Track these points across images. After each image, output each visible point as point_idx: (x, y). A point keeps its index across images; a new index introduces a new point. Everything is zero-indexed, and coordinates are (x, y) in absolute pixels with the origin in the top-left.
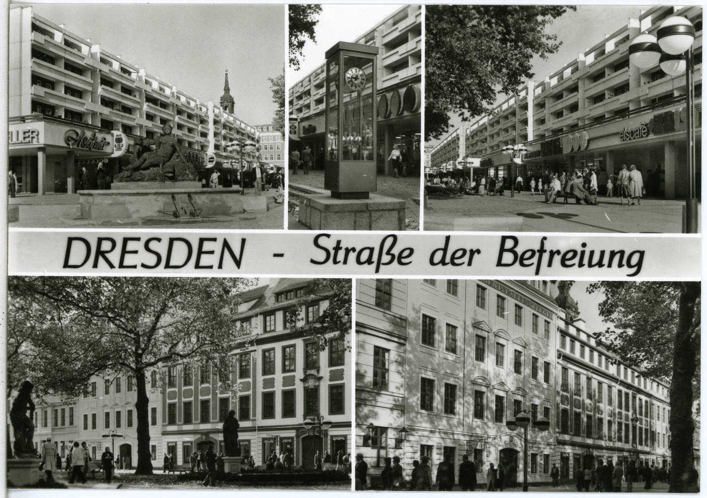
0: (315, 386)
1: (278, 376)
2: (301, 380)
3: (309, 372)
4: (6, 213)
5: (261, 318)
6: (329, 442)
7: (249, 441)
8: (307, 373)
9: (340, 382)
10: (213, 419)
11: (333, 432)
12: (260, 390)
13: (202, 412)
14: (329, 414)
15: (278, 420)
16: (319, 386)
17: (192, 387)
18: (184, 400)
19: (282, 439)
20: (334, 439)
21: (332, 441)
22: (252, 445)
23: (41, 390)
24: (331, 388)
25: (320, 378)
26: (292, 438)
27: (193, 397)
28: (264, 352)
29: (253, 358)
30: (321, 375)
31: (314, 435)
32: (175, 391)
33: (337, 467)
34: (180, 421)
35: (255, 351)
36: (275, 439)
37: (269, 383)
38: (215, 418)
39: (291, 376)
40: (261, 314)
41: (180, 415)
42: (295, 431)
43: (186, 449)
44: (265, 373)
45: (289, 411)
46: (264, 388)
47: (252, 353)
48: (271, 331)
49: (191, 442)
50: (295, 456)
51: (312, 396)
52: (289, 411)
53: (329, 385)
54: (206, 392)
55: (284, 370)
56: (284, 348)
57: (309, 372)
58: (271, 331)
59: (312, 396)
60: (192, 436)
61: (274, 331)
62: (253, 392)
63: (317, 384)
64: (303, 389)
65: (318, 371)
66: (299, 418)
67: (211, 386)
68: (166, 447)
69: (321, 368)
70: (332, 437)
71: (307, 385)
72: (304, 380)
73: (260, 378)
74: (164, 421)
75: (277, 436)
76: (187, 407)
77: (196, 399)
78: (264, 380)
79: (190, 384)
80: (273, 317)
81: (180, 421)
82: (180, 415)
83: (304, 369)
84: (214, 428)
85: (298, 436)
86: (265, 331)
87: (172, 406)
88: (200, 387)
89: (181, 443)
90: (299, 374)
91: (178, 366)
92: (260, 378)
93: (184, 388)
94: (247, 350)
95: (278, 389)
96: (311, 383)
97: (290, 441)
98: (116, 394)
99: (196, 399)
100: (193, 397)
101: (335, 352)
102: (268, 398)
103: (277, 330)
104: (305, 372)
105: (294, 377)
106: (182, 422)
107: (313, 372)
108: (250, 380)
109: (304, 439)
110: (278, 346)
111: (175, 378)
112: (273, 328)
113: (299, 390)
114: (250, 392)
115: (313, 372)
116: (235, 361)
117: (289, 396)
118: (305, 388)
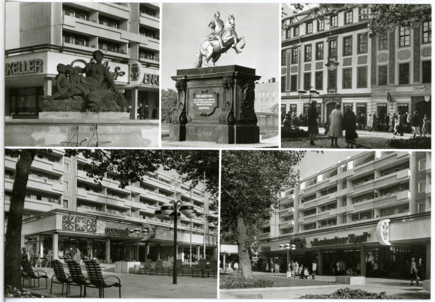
0: (334, 69)
1: (314, 62)
2: (326, 65)
3: (331, 60)
4: (4, 131)
5: (304, 24)
7: (296, 105)
8: (330, 60)
10: (287, 89)
12: (303, 71)
15: (354, 90)
16: (336, 69)
18: (291, 74)
21: (344, 107)
22: (298, 108)
24: (344, 70)
25: (337, 64)
27: (286, 73)
28: (306, 46)
29: (299, 51)
30: (338, 62)
31: (333, 102)
32: (285, 68)
33: (390, 130)
34: (288, 89)
35: (300, 46)
39: (364, 56)
40: (304, 22)
41: (288, 85)
42: (322, 99)
44: (344, 54)
45: (319, 86)
46: (305, 70)
47: (299, 48)
48: (310, 33)
53: (357, 67)
54: (294, 69)
55: (359, 52)
57: (331, 60)
58: (297, 35)
61: (312, 33)
63: (335, 68)
64: (327, 71)
65: (336, 59)
66: (324, 92)
70: (344, 104)
71: (330, 68)
72: (328, 65)
73: (303, 64)
76: (346, 73)
77: (288, 75)
78: (305, 65)
79: (296, 63)
81: (288, 89)
82: (288, 85)
83: (328, 58)
85: (324, 103)
86: (307, 33)
90: (325, 61)
91: (287, 50)
92: (303, 64)
93: (291, 66)
94: (296, 46)
95: (313, 71)
96: (332, 67)
99: (288, 75)
100: (286, 73)
101: (347, 46)
103: (325, 30)
104: (329, 60)
105: (322, 63)
106: (290, 90)
107: (333, 60)
108: (297, 65)
109: (328, 105)
110: (313, 42)
111: (285, 59)
112: (311, 32)
113: (325, 70)
114: (297, 73)
115: (333, 60)
116: (302, 49)
117: (319, 75)
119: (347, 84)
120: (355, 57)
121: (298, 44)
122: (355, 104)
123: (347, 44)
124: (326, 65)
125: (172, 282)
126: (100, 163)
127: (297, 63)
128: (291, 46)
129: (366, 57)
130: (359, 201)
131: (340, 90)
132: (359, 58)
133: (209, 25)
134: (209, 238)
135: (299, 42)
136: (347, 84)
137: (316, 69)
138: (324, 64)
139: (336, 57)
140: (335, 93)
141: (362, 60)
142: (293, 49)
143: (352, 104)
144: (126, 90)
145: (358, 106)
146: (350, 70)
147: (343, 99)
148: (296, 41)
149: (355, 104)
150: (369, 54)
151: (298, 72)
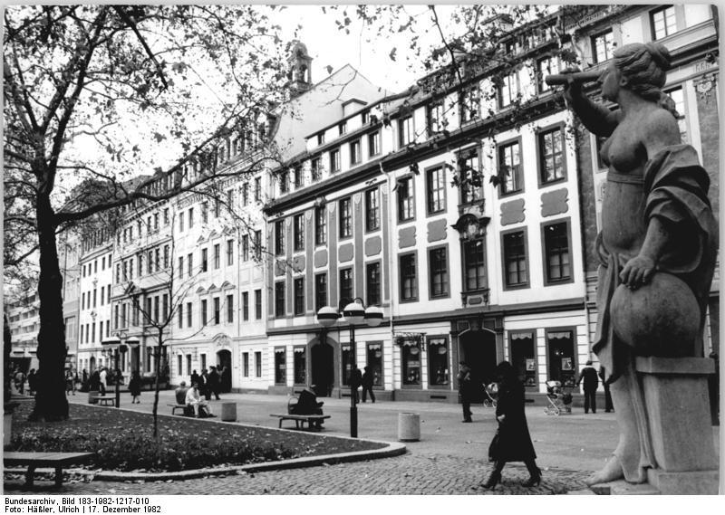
1: (533, 196)
3: (467, 211)
6: (506, 343)
8: (465, 213)
9: (519, 225)
11: (512, 324)
12: (396, 250)
13: (283, 300)
14: (504, 290)
15: (538, 290)
17: (352, 241)
19: (430, 338)
20: (514, 337)
23: (554, 149)
26: (445, 337)
30: (487, 214)
32: (378, 237)
35: (385, 181)
36: (418, 338)
37: (407, 237)
38: (290, 311)
42: (449, 324)
43: (298, 358)
45: (438, 291)
49: (304, 347)
50: (451, 372)
51: (474, 255)
52: (438, 291)
53: (501, 232)
56: (540, 135)
59: (474, 255)
60: (304, 336)
62: (357, 262)
67: (328, 250)
68: (273, 355)
69: (486, 202)
70: (511, 332)
71: (465, 235)
73: (395, 229)
74: (271, 312)
75: (423, 334)
78: (401, 232)
80: (411, 120)
83: (459, 206)
84: (310, 323)
87: (280, 286)
88: (314, 253)
89: (364, 345)
94: (375, 182)
97: (442, 341)
98: (214, 270)
102: (407, 263)
104: (461, 212)
108: (380, 234)
114: (381, 256)
115: (474, 210)
117: (438, 259)
118: (462, 240)
119: (513, 278)
121: (380, 178)
122: (541, 333)
128: (363, 185)
129: (565, 192)
131: (499, 296)
135: (380, 173)
136: (513, 278)
137: (504, 225)
138: (448, 226)
139: (481, 203)
143: (533, 332)
145: (551, 336)
148: (372, 171)
149: (541, 333)
150: (571, 185)
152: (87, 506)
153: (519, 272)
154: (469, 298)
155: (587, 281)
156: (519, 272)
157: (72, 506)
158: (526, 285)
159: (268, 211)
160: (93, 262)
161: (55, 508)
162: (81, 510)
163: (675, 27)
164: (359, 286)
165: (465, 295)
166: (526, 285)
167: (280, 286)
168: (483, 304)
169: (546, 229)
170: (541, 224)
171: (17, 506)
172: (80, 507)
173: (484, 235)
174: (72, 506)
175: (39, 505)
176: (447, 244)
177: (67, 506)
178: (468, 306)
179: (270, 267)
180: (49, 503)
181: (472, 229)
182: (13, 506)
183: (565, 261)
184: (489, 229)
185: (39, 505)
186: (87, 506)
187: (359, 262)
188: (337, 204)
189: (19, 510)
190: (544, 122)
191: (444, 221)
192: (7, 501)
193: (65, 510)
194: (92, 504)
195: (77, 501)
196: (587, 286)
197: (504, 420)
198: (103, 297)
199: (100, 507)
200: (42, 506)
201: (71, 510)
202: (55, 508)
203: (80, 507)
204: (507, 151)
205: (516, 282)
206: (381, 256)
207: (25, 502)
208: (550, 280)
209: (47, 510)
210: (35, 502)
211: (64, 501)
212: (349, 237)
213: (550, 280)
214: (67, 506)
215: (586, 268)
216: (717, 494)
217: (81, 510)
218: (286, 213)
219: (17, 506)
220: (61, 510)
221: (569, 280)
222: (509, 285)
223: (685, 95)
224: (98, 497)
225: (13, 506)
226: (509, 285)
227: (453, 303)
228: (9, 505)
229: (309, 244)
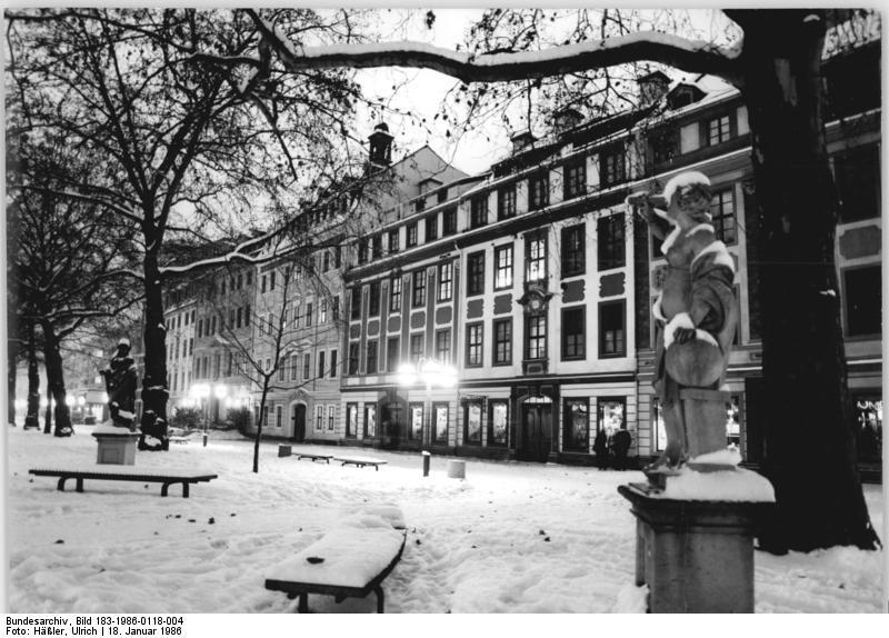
2: (519, 302)
15: (592, 362)
35: (458, 257)
42: (509, 389)
46: (469, 316)
53: (599, 303)
56: (497, 250)
60: (375, 393)
74: (345, 370)
78: (470, 304)
114: (451, 324)
119: (573, 350)
120: (592, 278)
121: (453, 254)
123: (475, 269)
124: (519, 302)
125: (181, 492)
126: (142, 267)
127: (424, 305)
128: (436, 259)
129: (622, 275)
130: (10, 268)
131: (557, 366)
132: (603, 279)
133: (68, 435)
134: (16, 100)
136: (573, 350)
138: (513, 300)
140: (541, 373)
141: (611, 285)
142: (440, 264)
144: (669, 456)
146: (581, 311)
147: (563, 387)
148: (449, 246)
150: (629, 270)
151: (379, 335)
152: (106, 627)
153: (576, 344)
154: (529, 366)
155: (637, 356)
156: (576, 344)
157: (88, 627)
158: (583, 357)
159: (346, 278)
160: (176, 317)
161: (67, 629)
162: (100, 632)
163: (728, 135)
164: (363, 355)
165: (525, 366)
166: (583, 357)
167: (354, 347)
168: (541, 373)
169: (603, 308)
170: (599, 303)
171: (22, 627)
172: (99, 628)
173: (547, 308)
174: (88, 627)
175: (48, 625)
176: (584, 306)
177: (82, 627)
178: (528, 373)
179: (346, 332)
180: (60, 623)
181: (536, 304)
182: (16, 627)
183: (580, 341)
184: (552, 303)
185: (48, 625)
186: (106, 627)
187: (383, 337)
188: (368, 286)
189: (24, 632)
190: (605, 213)
191: (510, 296)
192: (9, 620)
193: (80, 631)
194: (113, 625)
195: (94, 622)
196: (638, 361)
197: (760, 542)
198: (185, 349)
199: (123, 629)
200: (52, 627)
201: (86, 632)
202: (67, 629)
203: (99, 628)
204: (502, 254)
205: (573, 353)
206: (451, 324)
207: (31, 622)
208: (496, 362)
209: (57, 632)
210: (43, 622)
211: (78, 621)
212: (420, 305)
213: (496, 362)
214: (82, 627)
215: (638, 346)
216: (749, 609)
217: (100, 632)
218: (363, 280)
219: (22, 627)
220: (75, 631)
221: (623, 354)
222: (565, 357)
223: (734, 196)
224: (121, 616)
225: (16, 627)
226: (565, 357)
227: (515, 370)
228: (11, 625)
229: (365, 315)
